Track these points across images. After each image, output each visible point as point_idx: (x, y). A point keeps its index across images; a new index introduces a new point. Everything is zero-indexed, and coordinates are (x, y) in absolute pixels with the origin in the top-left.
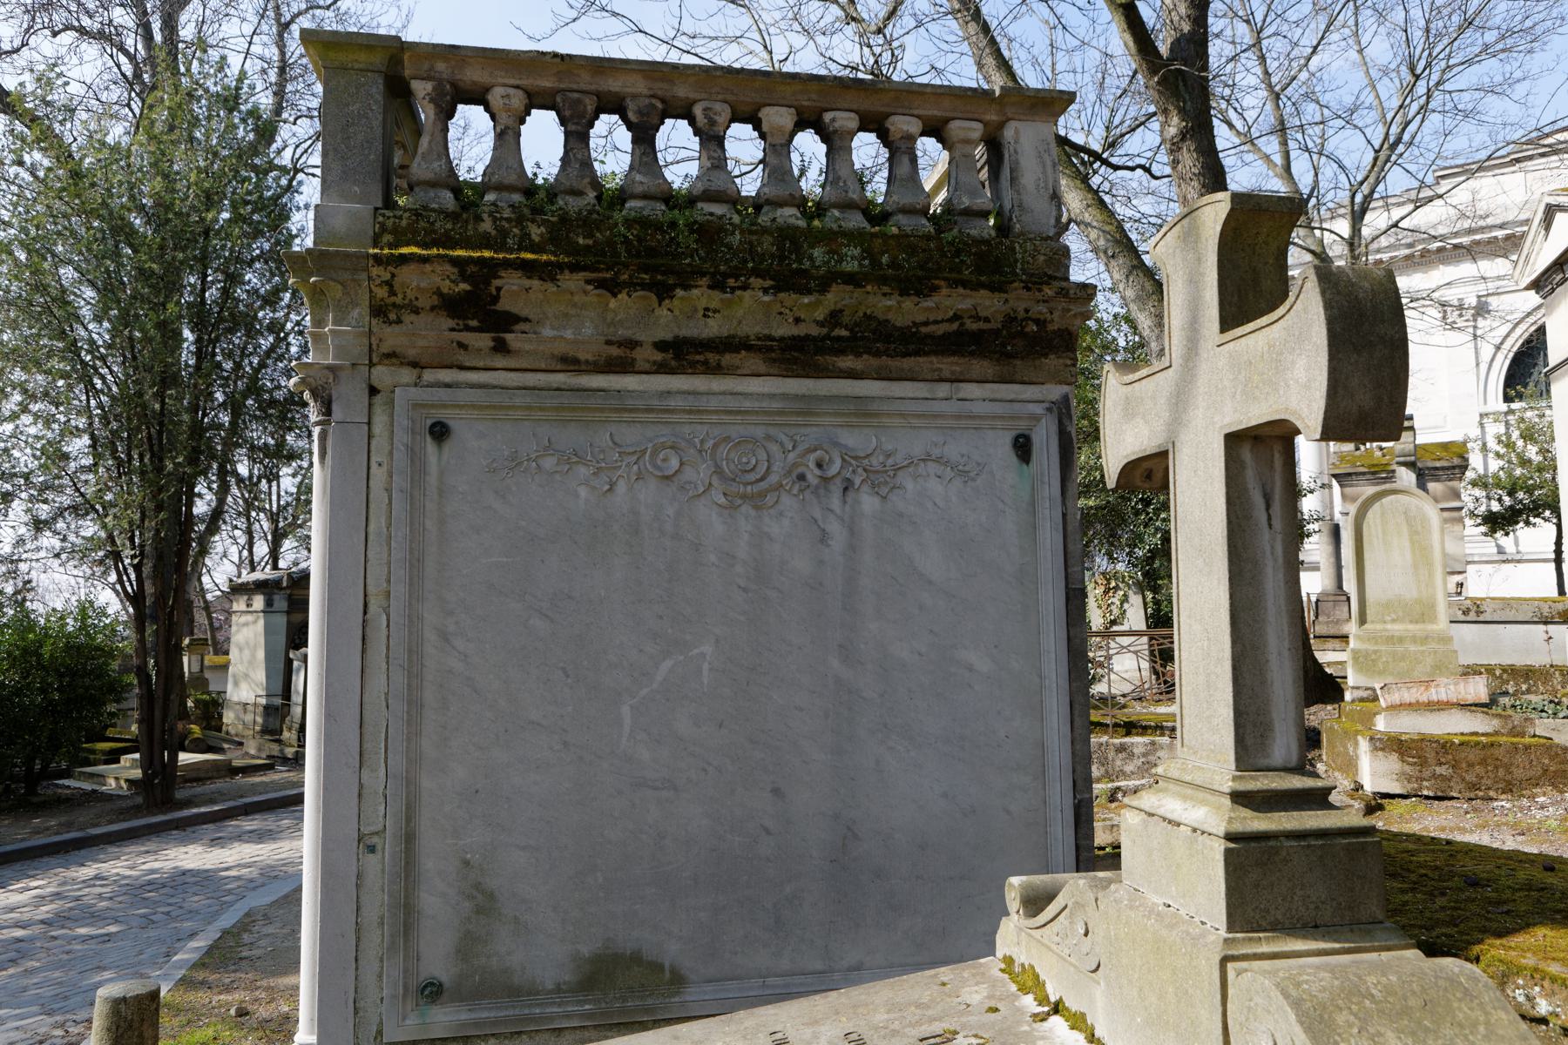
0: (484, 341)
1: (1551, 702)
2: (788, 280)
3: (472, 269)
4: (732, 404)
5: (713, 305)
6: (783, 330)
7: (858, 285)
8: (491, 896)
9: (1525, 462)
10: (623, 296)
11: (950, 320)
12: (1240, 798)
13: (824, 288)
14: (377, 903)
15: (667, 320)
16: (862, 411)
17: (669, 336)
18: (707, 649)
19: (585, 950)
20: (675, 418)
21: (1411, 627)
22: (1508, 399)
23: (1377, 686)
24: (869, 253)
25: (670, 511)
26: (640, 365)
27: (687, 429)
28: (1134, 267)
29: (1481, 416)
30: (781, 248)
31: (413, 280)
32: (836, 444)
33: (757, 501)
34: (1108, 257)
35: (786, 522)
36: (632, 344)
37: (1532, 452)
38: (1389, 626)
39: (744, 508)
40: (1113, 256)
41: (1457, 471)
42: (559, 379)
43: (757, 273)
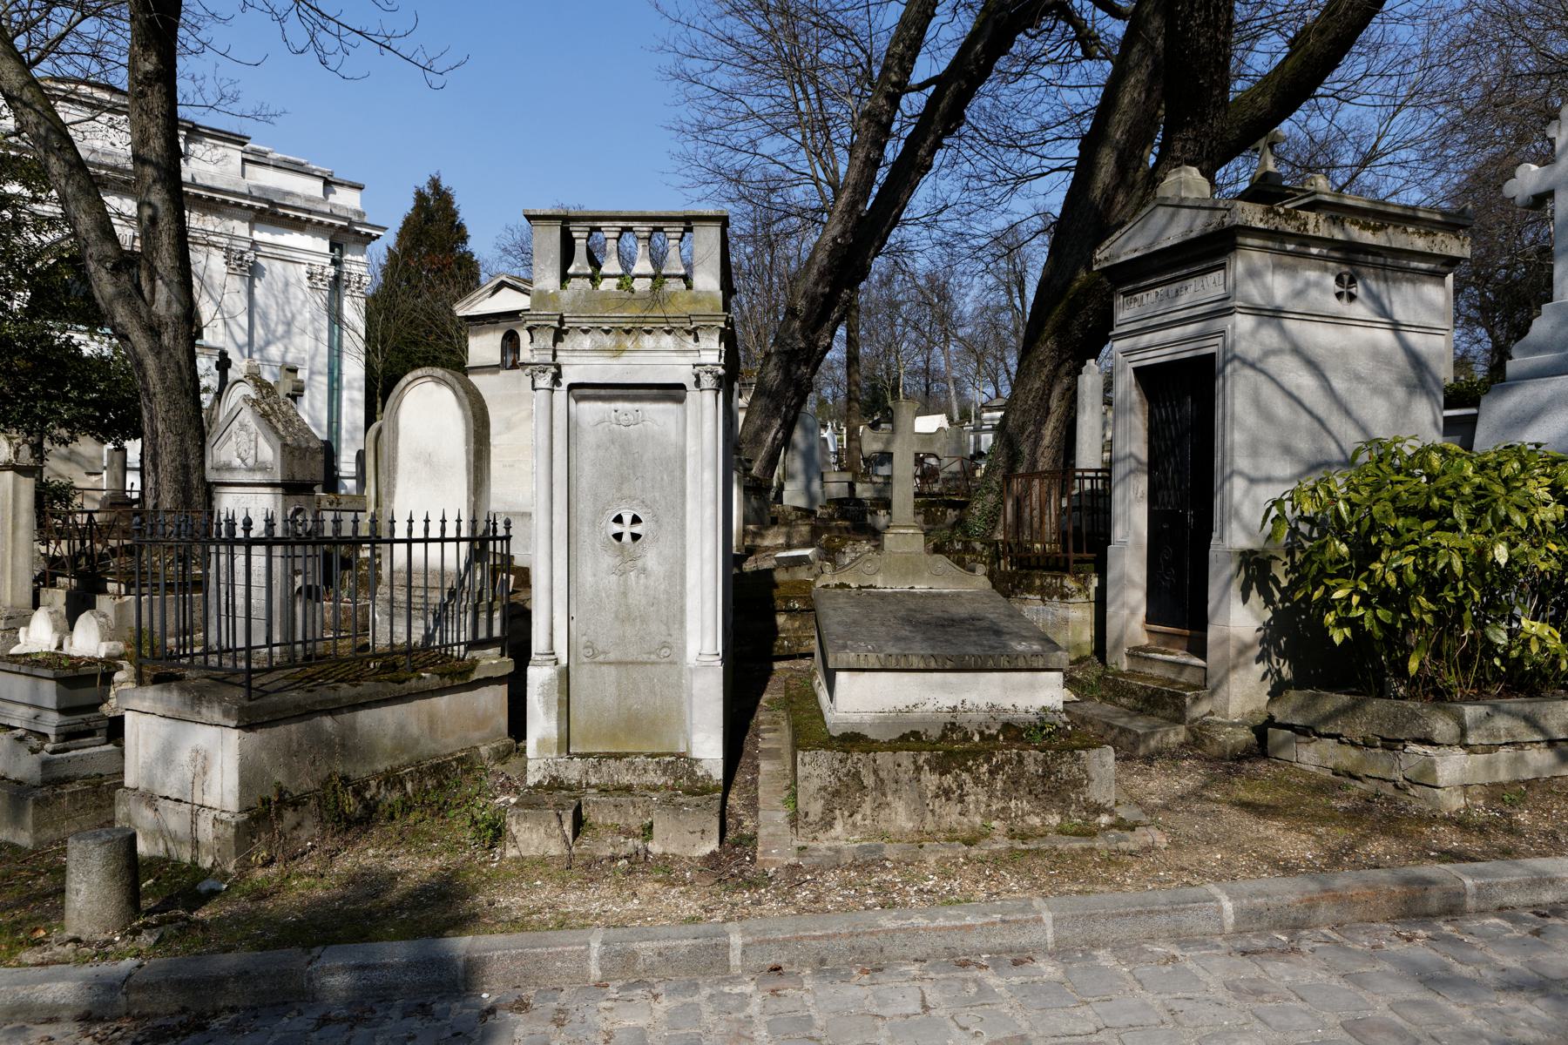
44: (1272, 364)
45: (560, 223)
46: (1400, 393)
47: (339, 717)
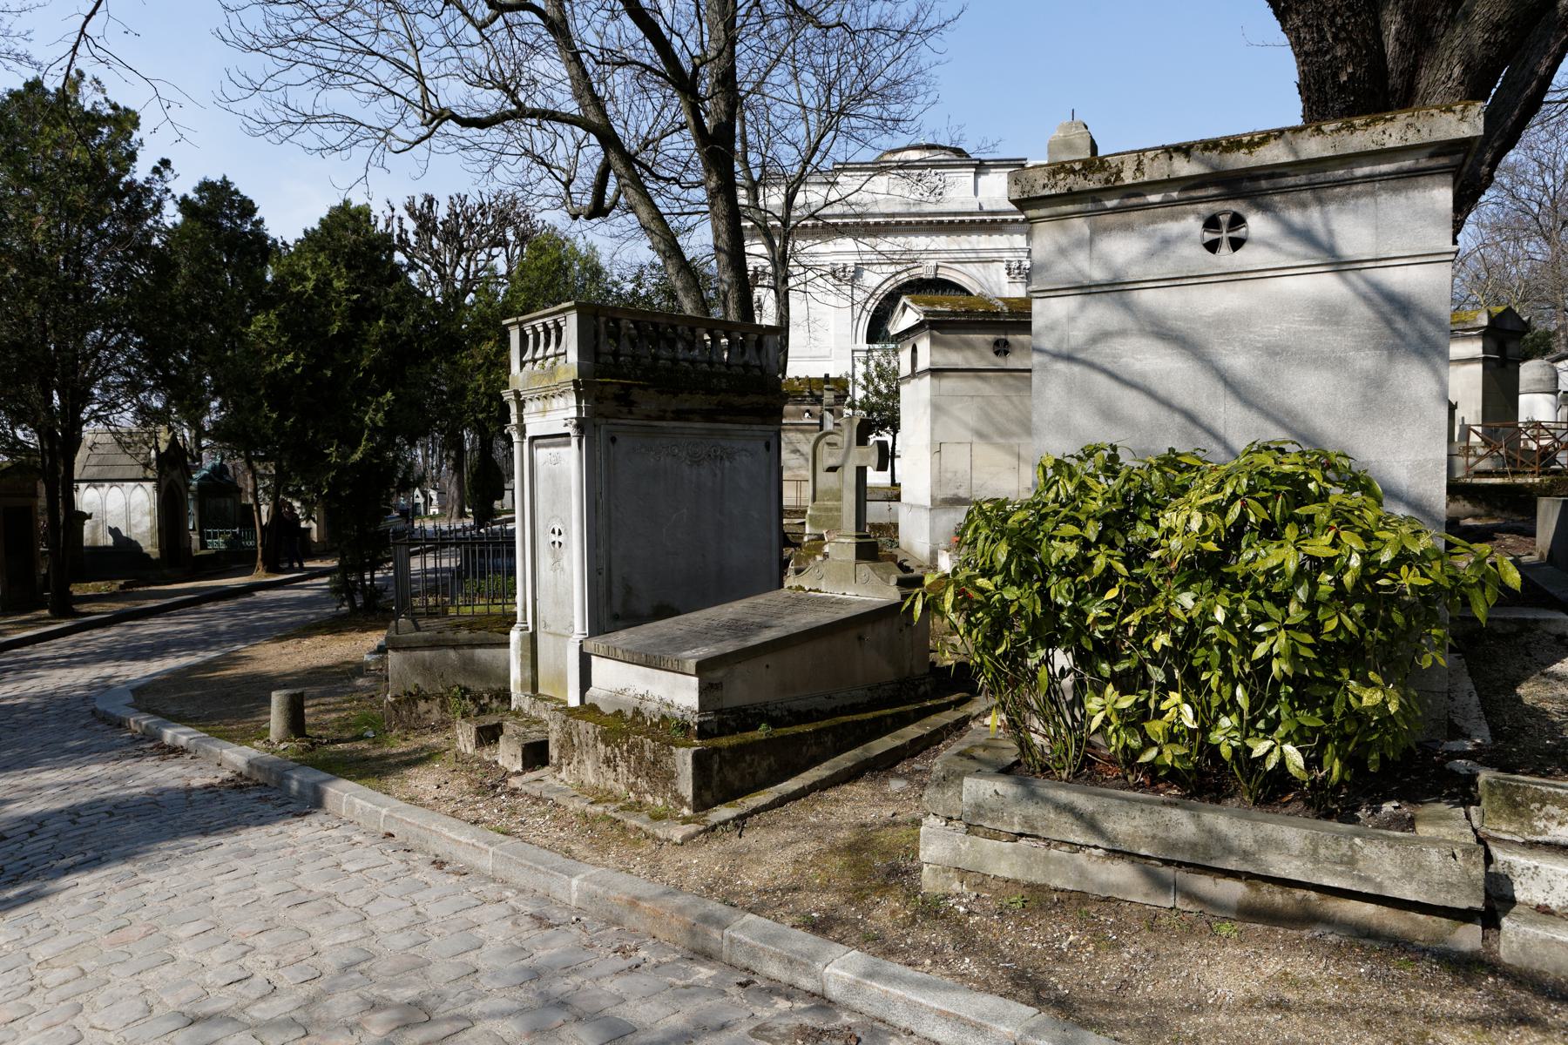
0: (625, 410)
2: (710, 391)
6: (706, 407)
9: (878, 393)
22: (868, 342)
28: (682, 267)
33: (698, 463)
36: (665, 411)
37: (882, 387)
42: (645, 422)
44: (1103, 353)
46: (1367, 360)
47: (461, 651)
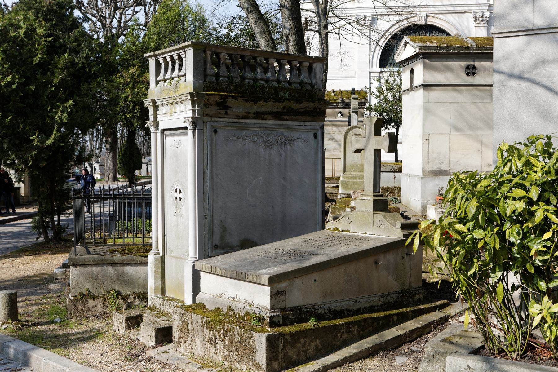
0: (223, 112)
1: (395, 198)
2: (278, 100)
3: (223, 97)
4: (266, 126)
5: (264, 105)
7: (289, 101)
8: (225, 228)
9: (387, 100)
10: (248, 103)
11: (304, 108)
12: (374, 196)
13: (283, 102)
14: (207, 229)
15: (255, 108)
16: (288, 128)
17: (255, 111)
18: (261, 178)
19: (241, 239)
20: (256, 129)
21: (359, 173)
23: (351, 192)
24: (290, 93)
25: (255, 149)
26: (251, 117)
27: (258, 131)
28: (259, 18)
29: (370, 73)
30: (275, 92)
31: (213, 99)
32: (284, 135)
33: (270, 147)
34: (248, 12)
35: (275, 151)
36: (249, 113)
38: (352, 173)
39: (268, 148)
40: (250, 12)
41: (363, 105)
42: (236, 120)
43: (273, 98)
45: (154, 58)
47: (116, 268)
